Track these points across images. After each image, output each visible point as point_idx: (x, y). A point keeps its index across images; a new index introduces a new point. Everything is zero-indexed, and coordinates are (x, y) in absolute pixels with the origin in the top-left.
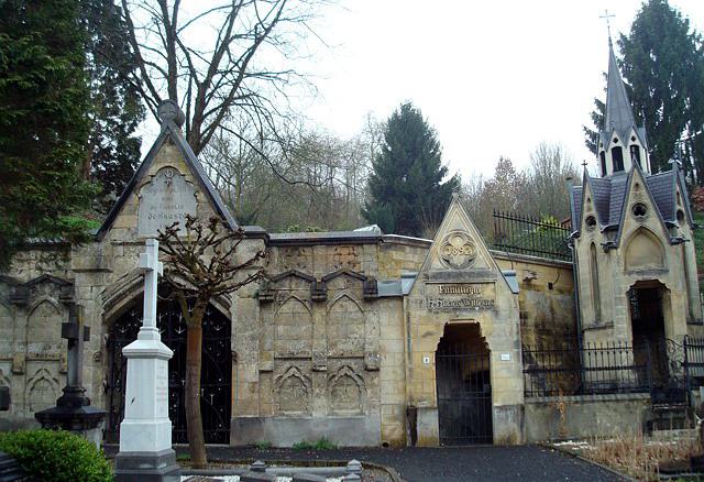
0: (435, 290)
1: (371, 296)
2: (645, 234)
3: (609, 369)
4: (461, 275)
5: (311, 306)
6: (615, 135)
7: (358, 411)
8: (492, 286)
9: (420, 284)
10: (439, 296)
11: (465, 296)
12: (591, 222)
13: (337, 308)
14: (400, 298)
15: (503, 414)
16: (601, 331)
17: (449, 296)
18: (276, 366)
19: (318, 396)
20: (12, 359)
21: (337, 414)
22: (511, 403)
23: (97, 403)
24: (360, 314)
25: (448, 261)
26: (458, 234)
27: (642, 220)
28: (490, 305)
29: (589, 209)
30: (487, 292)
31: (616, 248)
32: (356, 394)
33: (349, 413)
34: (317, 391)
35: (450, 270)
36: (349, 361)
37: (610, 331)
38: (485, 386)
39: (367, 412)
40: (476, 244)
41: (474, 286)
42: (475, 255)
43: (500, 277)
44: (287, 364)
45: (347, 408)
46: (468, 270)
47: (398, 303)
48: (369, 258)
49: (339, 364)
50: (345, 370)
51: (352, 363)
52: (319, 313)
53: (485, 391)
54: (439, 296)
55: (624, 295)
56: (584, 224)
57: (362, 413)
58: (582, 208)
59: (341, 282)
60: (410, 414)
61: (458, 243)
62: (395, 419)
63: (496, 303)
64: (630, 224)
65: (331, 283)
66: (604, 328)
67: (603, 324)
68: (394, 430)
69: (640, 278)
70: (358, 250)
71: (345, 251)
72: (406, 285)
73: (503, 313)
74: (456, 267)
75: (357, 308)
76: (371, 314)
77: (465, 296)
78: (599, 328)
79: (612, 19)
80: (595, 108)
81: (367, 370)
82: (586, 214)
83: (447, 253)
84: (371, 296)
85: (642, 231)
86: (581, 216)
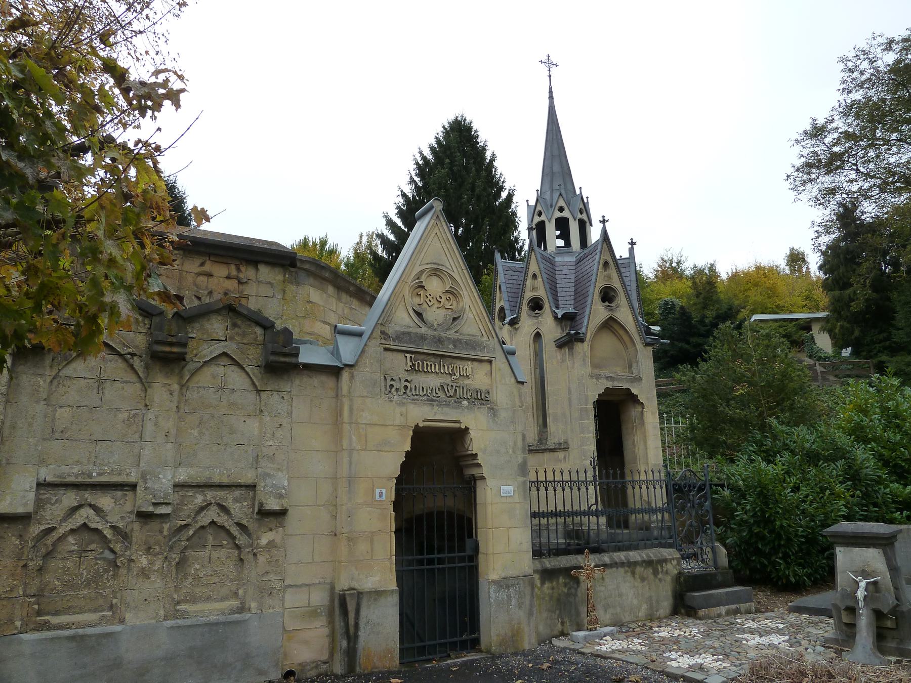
0: (399, 364)
1: (280, 362)
2: (614, 333)
3: (556, 514)
4: (439, 341)
5: (147, 367)
6: (561, 203)
7: (234, 603)
8: (486, 366)
9: (375, 349)
10: (405, 376)
11: (447, 380)
12: (536, 305)
13: (205, 377)
14: (335, 371)
15: (503, 595)
16: (547, 455)
17: (431, 376)
18: (39, 503)
19: (144, 573)
20: (252, 487)
21: (184, 615)
22: (515, 573)
23: (96, 204)
24: (251, 396)
25: (419, 315)
26: (436, 272)
27: (611, 310)
28: (481, 399)
29: (534, 289)
30: (479, 377)
31: (582, 341)
32: (230, 568)
33: (212, 610)
34: (144, 561)
35: (424, 330)
36: (221, 493)
37: (561, 455)
38: (468, 542)
39: (253, 605)
40: (464, 293)
41: (459, 364)
42: (463, 310)
43: (499, 355)
44: (70, 499)
45: (208, 599)
46: (451, 334)
47: (330, 382)
48: (266, 290)
49: (199, 500)
50: (212, 514)
51: (229, 499)
52: (163, 389)
53: (469, 552)
54: (405, 376)
55: (590, 406)
56: (525, 308)
57: (242, 609)
58: (524, 284)
59: (217, 326)
60: (344, 608)
61: (435, 286)
62: (313, 613)
63: (493, 397)
64: (598, 313)
65: (197, 325)
66: (553, 450)
67: (551, 444)
68: (310, 645)
69: (610, 385)
70: (248, 272)
71: (220, 271)
72: (348, 350)
73: (503, 415)
74: (431, 327)
75: (247, 384)
76: (276, 397)
77: (447, 380)
78: (544, 451)
79: (553, 69)
80: (401, 201)
81: (264, 514)
82: (529, 295)
83: (417, 300)
84: (280, 362)
85: (610, 325)
86: (522, 295)
